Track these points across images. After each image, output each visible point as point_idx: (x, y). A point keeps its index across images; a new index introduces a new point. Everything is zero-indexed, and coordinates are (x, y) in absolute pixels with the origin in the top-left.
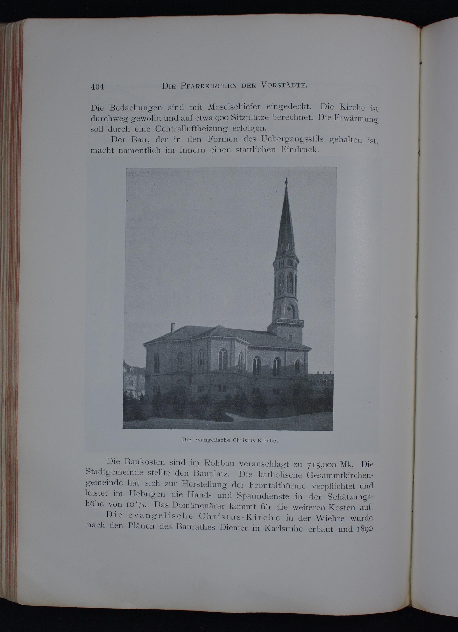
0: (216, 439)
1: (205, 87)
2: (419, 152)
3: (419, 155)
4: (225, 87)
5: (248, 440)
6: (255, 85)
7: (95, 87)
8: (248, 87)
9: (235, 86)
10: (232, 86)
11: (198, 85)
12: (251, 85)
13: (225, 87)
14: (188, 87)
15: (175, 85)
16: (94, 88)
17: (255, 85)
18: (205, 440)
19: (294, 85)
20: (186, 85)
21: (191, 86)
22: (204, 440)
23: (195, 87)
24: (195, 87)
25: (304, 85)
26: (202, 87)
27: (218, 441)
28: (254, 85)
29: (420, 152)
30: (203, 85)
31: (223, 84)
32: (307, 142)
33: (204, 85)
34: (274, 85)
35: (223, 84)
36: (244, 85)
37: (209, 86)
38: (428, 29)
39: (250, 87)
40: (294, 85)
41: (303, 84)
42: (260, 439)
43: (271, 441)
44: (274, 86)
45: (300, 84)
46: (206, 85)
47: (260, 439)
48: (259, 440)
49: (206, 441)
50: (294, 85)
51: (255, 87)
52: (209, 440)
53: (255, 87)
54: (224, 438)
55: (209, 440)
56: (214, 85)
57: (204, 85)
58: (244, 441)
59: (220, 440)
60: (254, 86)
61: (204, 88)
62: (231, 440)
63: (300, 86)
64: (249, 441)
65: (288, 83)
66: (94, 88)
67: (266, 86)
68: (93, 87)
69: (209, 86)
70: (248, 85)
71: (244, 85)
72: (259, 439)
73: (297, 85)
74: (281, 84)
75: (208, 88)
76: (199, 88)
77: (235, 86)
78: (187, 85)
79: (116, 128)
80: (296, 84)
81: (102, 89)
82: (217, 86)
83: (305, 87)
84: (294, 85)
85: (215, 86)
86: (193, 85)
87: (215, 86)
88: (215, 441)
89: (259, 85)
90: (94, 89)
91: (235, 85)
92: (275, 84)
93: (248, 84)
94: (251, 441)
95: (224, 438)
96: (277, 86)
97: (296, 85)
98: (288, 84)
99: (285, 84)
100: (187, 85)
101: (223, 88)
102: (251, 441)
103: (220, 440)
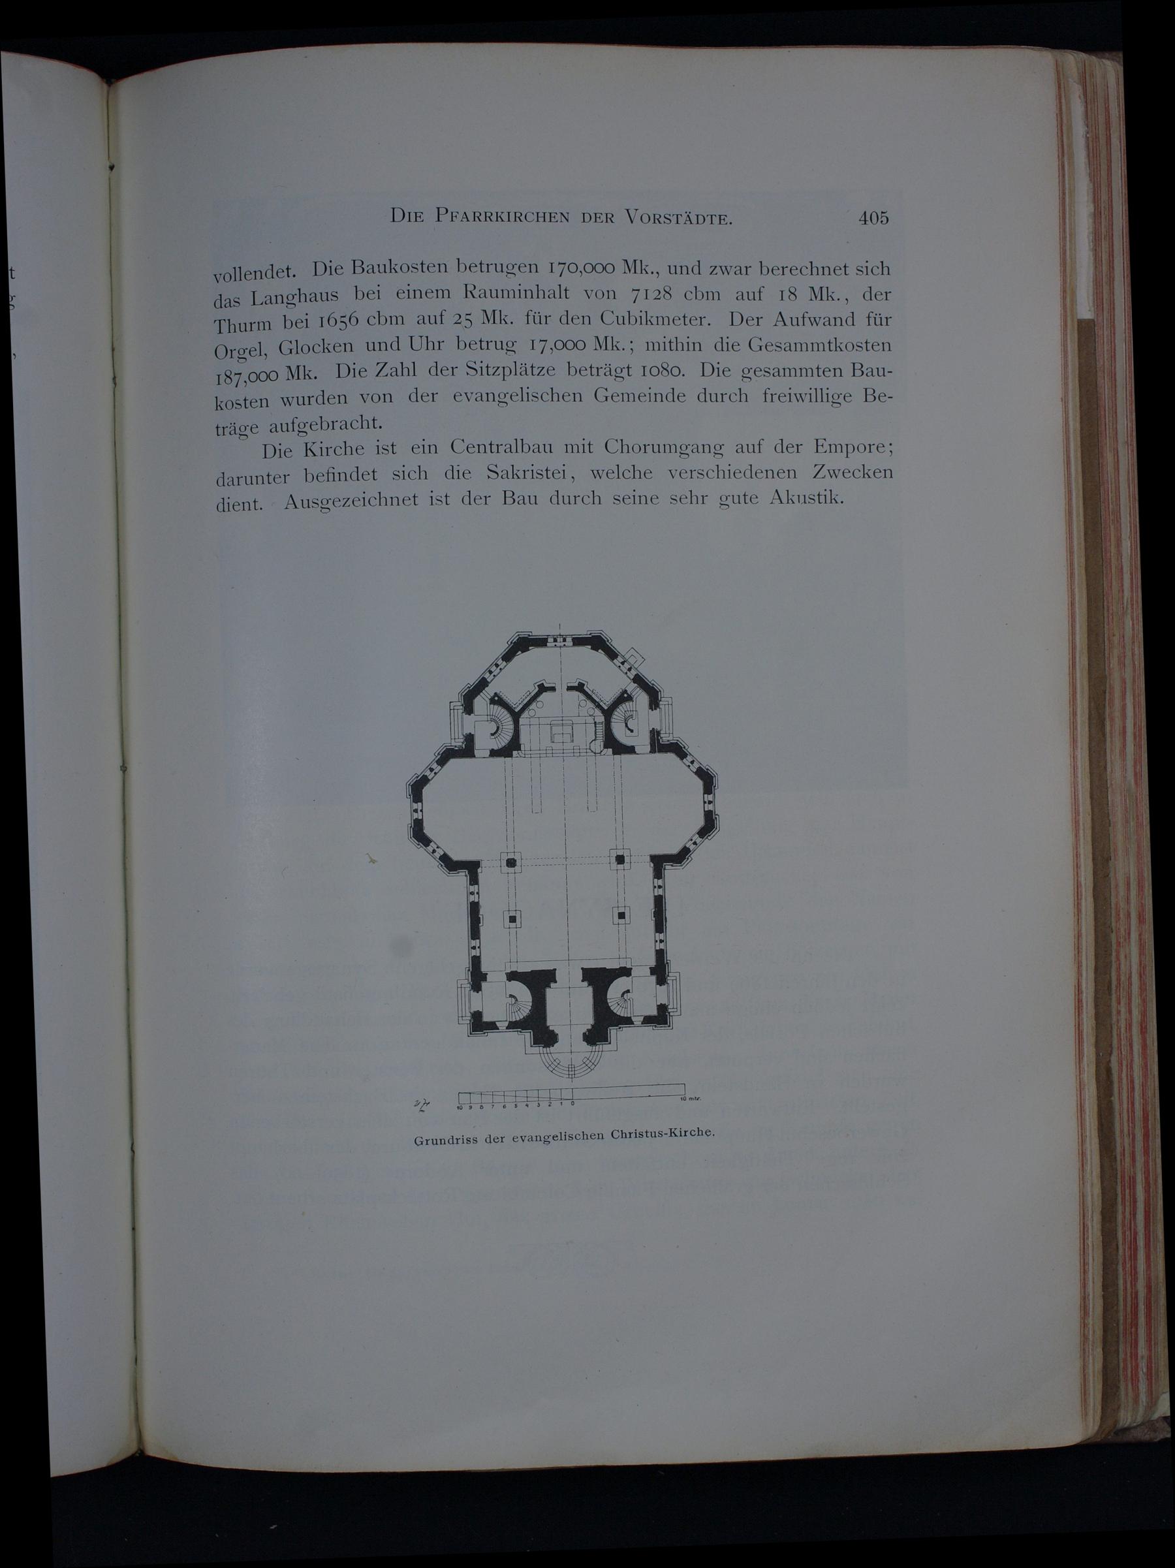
0: (563, 1134)
1: (494, 218)
2: (114, 378)
3: (115, 384)
4: (541, 219)
5: (647, 1132)
6: (613, 216)
7: (868, 218)
8: (596, 221)
9: (564, 216)
10: (558, 217)
11: (477, 214)
12: (603, 218)
13: (541, 219)
14: (454, 218)
15: (726, 216)
16: (865, 221)
17: (613, 216)
18: (538, 1138)
19: (701, 219)
20: (449, 213)
21: (460, 216)
22: (534, 1138)
23: (471, 217)
24: (471, 217)
25: (600, 218)
26: (488, 219)
27: (567, 1137)
28: (609, 216)
29: (117, 379)
30: (489, 214)
31: (538, 213)
32: (764, 366)
33: (492, 214)
34: (452, 216)
35: (538, 213)
36: (587, 218)
37: (505, 217)
38: (129, 87)
39: (726, 224)
40: (700, 219)
41: (722, 217)
42: (675, 1129)
43: (700, 1133)
44: (656, 221)
45: (681, 215)
46: (497, 213)
47: (675, 1129)
48: (672, 1133)
49: (540, 1140)
50: (700, 219)
51: (612, 222)
52: (546, 1137)
53: (612, 222)
54: (583, 1132)
55: (546, 1137)
56: (656, 216)
57: (492, 214)
58: (638, 1135)
59: (574, 1137)
60: (609, 218)
61: (480, 220)
62: (607, 1135)
63: (716, 220)
64: (649, 1134)
65: (688, 213)
66: (865, 221)
67: (637, 220)
68: (863, 219)
69: (505, 217)
70: (596, 217)
71: (587, 218)
72: (671, 1129)
73: (708, 219)
74: (672, 215)
75: (503, 221)
76: (613, 221)
77: (564, 216)
78: (452, 213)
79: (245, 324)
80: (705, 216)
81: (865, 224)
82: (523, 218)
83: (557, 221)
84: (701, 219)
85: (518, 217)
86: (465, 213)
87: (518, 217)
88: (599, 1138)
89: (621, 218)
90: (867, 222)
91: (566, 215)
92: (657, 217)
93: (596, 214)
94: (653, 1135)
95: (583, 1132)
96: (662, 220)
97: (706, 218)
98: (688, 216)
99: (681, 215)
100: (452, 213)
101: (538, 221)
102: (653, 1135)
103: (574, 1137)
